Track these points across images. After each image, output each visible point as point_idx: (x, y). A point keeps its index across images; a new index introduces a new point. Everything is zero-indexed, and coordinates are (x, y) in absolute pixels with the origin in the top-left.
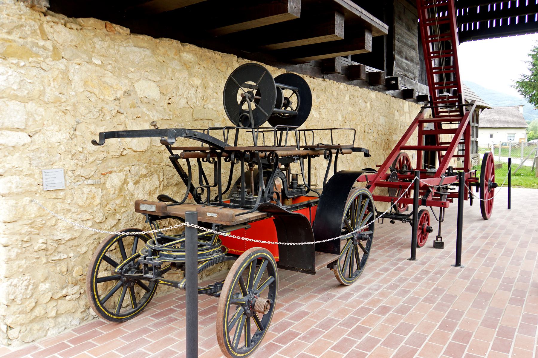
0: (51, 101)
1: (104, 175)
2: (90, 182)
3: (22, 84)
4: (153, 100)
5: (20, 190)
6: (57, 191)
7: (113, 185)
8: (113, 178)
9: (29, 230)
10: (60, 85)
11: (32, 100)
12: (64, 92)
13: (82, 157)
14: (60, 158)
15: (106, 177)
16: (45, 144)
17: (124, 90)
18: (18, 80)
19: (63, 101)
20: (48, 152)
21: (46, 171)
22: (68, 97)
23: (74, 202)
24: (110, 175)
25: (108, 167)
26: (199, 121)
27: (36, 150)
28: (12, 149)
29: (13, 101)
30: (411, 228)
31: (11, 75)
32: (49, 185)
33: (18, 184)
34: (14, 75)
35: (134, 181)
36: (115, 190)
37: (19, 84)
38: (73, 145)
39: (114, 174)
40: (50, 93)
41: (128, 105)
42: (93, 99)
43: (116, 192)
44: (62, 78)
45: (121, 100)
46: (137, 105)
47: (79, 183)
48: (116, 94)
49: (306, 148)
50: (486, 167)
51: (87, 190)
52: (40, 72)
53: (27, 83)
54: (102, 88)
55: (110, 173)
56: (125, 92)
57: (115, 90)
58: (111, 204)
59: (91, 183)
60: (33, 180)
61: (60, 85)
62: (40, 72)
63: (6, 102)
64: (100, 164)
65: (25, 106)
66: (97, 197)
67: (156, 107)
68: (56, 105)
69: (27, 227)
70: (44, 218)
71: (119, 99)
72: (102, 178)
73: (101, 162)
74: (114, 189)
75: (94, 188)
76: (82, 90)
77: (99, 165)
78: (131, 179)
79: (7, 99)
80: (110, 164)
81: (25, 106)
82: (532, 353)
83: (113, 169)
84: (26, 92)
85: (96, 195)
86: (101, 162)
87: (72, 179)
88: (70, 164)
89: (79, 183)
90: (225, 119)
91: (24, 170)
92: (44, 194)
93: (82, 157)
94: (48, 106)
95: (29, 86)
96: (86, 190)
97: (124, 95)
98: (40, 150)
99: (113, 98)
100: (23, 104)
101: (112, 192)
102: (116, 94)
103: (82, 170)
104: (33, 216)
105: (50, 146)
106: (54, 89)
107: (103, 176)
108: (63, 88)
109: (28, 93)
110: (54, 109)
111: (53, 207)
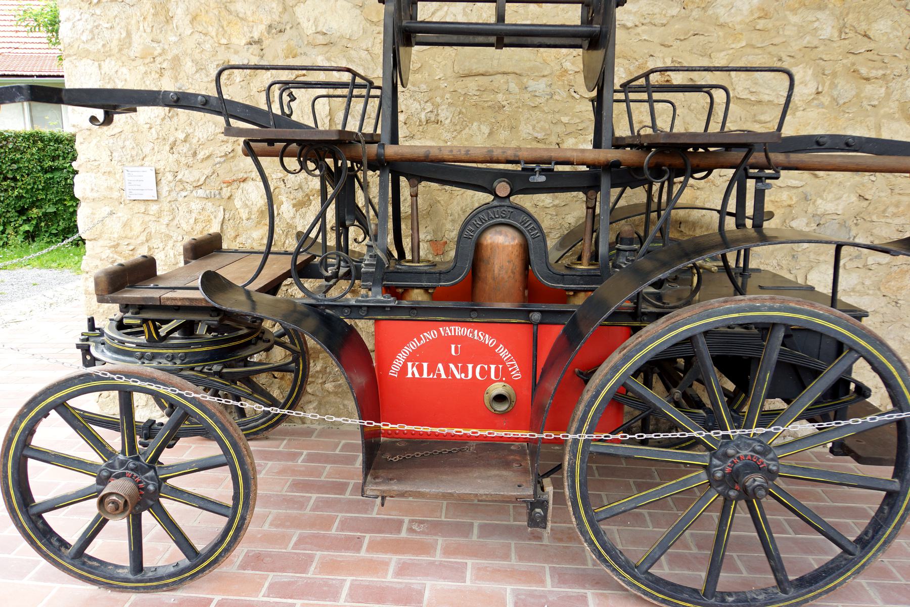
0: (138, 55)
1: (229, 184)
2: (201, 192)
3: (96, 31)
4: (342, 37)
5: (95, 195)
6: (149, 203)
7: (249, 203)
8: (250, 191)
9: (111, 255)
10: (153, 27)
11: (110, 56)
12: (161, 37)
13: (184, 148)
14: (153, 149)
15: (233, 187)
16: (129, 126)
17: (269, 22)
18: (89, 27)
19: (156, 53)
20: (135, 140)
21: (130, 169)
22: (166, 47)
23: (175, 222)
24: (242, 184)
25: (238, 170)
26: (477, 78)
27: (116, 136)
28: (88, 133)
29: (84, 60)
30: (854, 365)
31: (79, 20)
32: (134, 192)
33: (93, 185)
34: (84, 19)
35: (294, 201)
36: (250, 213)
37: (91, 31)
38: (173, 129)
39: (251, 183)
40: (140, 41)
41: (280, 51)
42: (207, 46)
43: (253, 217)
44: (153, 15)
45: (266, 43)
46: (299, 51)
47: (184, 194)
48: (251, 32)
49: (637, 144)
50: (480, 165)
51: (197, 206)
52: (125, 9)
53: (104, 30)
54: (225, 23)
55: (244, 180)
56: (270, 26)
57: (251, 24)
58: (244, 236)
59: (202, 195)
60: (114, 181)
61: (153, 27)
62: (125, 9)
63: (75, 62)
64: (219, 163)
65: (100, 66)
66: (214, 220)
67: (352, 52)
68: (147, 61)
69: (109, 251)
70: (132, 241)
71: (259, 42)
72: (224, 190)
73: (222, 160)
74: (247, 210)
75: (210, 204)
76: (191, 31)
77: (217, 166)
78: (286, 195)
79: (74, 57)
80: (242, 165)
81: (100, 66)
82: (564, 493)
83: (248, 175)
84: (102, 43)
85: (212, 217)
86: (222, 160)
87: (172, 184)
88: (165, 160)
89: (184, 194)
90: (566, 71)
91: (101, 165)
92: (131, 205)
93: (184, 148)
94: (134, 64)
95: (107, 34)
96: (196, 206)
97: (269, 33)
98: (123, 136)
99: (244, 42)
100: (96, 64)
101: (244, 216)
102: (251, 32)
103: (186, 172)
104: (116, 235)
105: (135, 129)
106: (144, 35)
107: (225, 185)
108: (158, 31)
109: (104, 45)
110: (143, 69)
111: (144, 227)
